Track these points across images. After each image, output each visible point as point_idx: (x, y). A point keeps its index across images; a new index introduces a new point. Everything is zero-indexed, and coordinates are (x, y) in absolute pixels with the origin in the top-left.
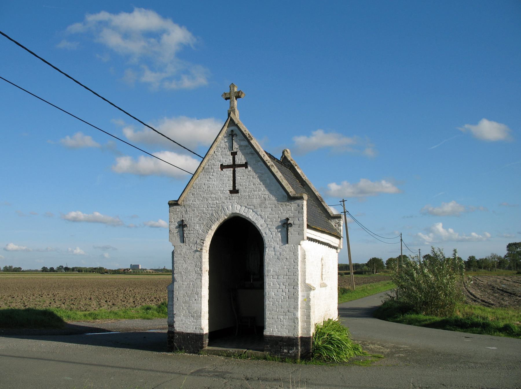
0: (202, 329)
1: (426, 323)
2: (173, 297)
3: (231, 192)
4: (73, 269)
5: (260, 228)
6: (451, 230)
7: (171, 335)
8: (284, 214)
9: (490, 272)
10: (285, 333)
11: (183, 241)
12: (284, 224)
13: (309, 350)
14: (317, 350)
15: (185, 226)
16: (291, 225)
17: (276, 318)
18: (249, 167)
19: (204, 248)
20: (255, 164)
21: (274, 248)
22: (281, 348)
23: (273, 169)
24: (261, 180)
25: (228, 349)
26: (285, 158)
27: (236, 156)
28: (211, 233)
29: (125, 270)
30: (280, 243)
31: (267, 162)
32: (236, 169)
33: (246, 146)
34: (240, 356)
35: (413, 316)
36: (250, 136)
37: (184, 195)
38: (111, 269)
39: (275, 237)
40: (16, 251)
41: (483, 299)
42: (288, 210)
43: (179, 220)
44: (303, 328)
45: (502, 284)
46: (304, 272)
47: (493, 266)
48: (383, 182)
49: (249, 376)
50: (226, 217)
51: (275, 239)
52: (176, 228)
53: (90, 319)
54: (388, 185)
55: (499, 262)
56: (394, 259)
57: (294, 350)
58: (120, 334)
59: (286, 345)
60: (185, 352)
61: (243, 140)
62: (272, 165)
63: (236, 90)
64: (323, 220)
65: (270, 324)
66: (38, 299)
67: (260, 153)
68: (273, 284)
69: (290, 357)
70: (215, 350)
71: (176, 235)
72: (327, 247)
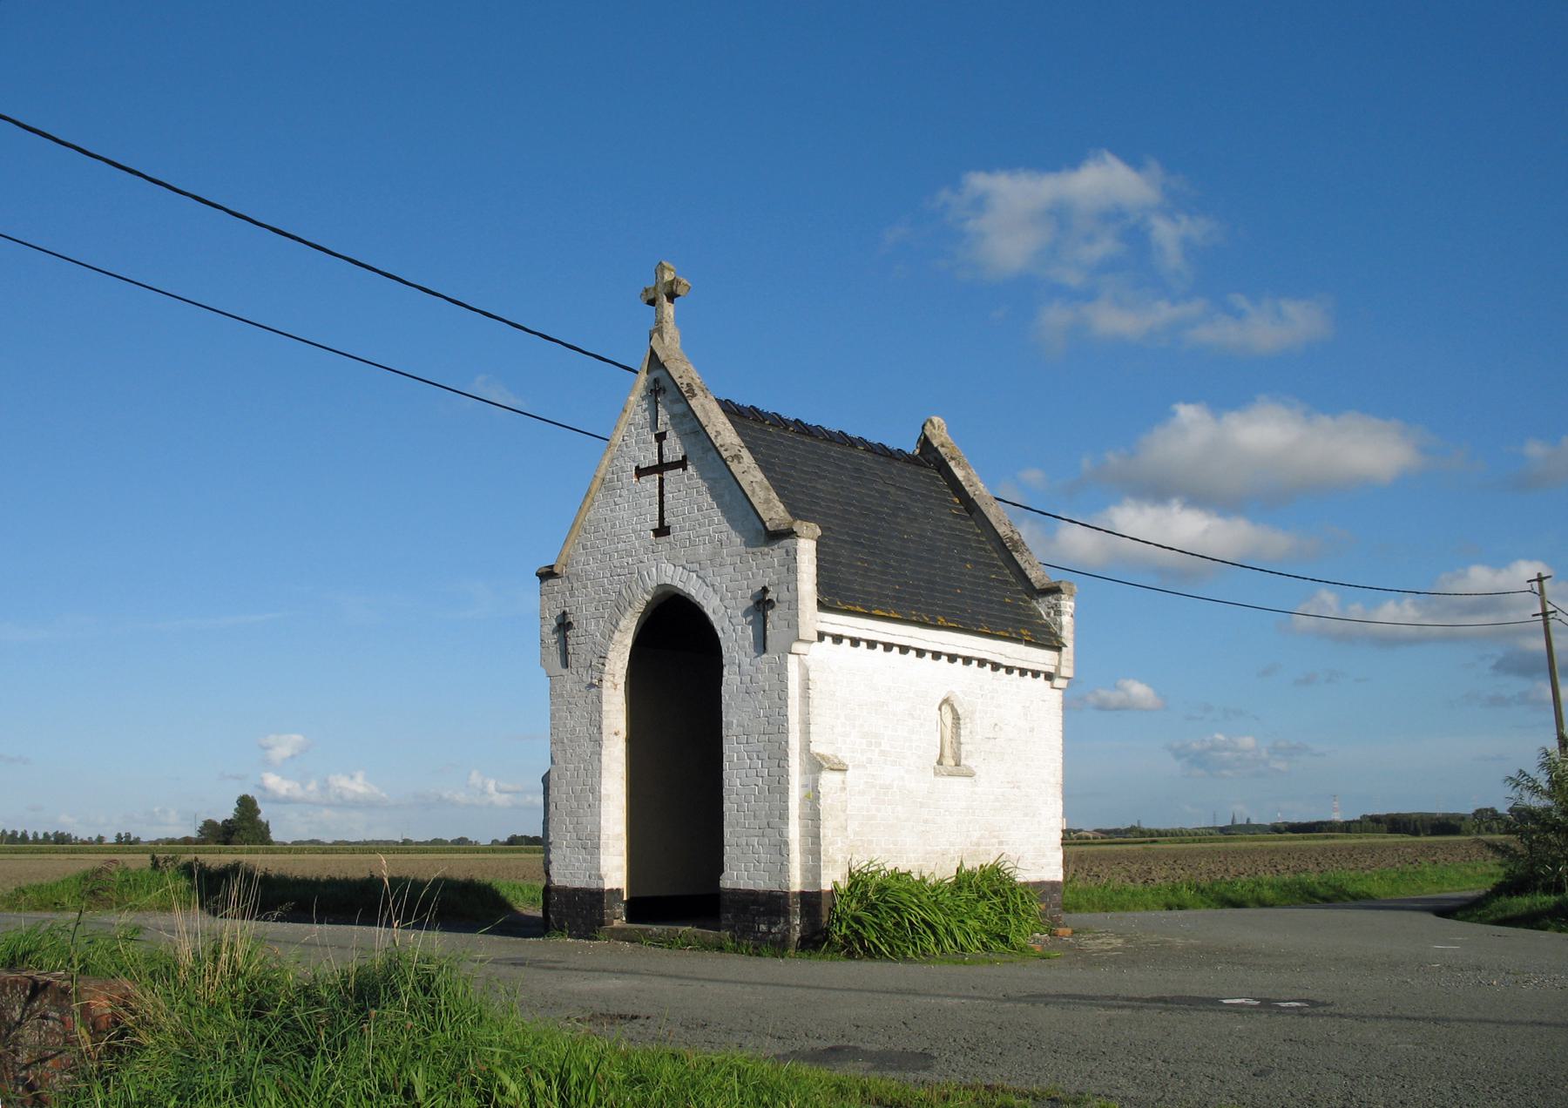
0: (600, 878)
11: (566, 664)
19: (606, 677)
23: (734, 466)
24: (714, 498)
26: (925, 443)
30: (750, 651)
42: (762, 568)
50: (649, 598)
60: (570, 936)
63: (668, 277)
69: (773, 943)
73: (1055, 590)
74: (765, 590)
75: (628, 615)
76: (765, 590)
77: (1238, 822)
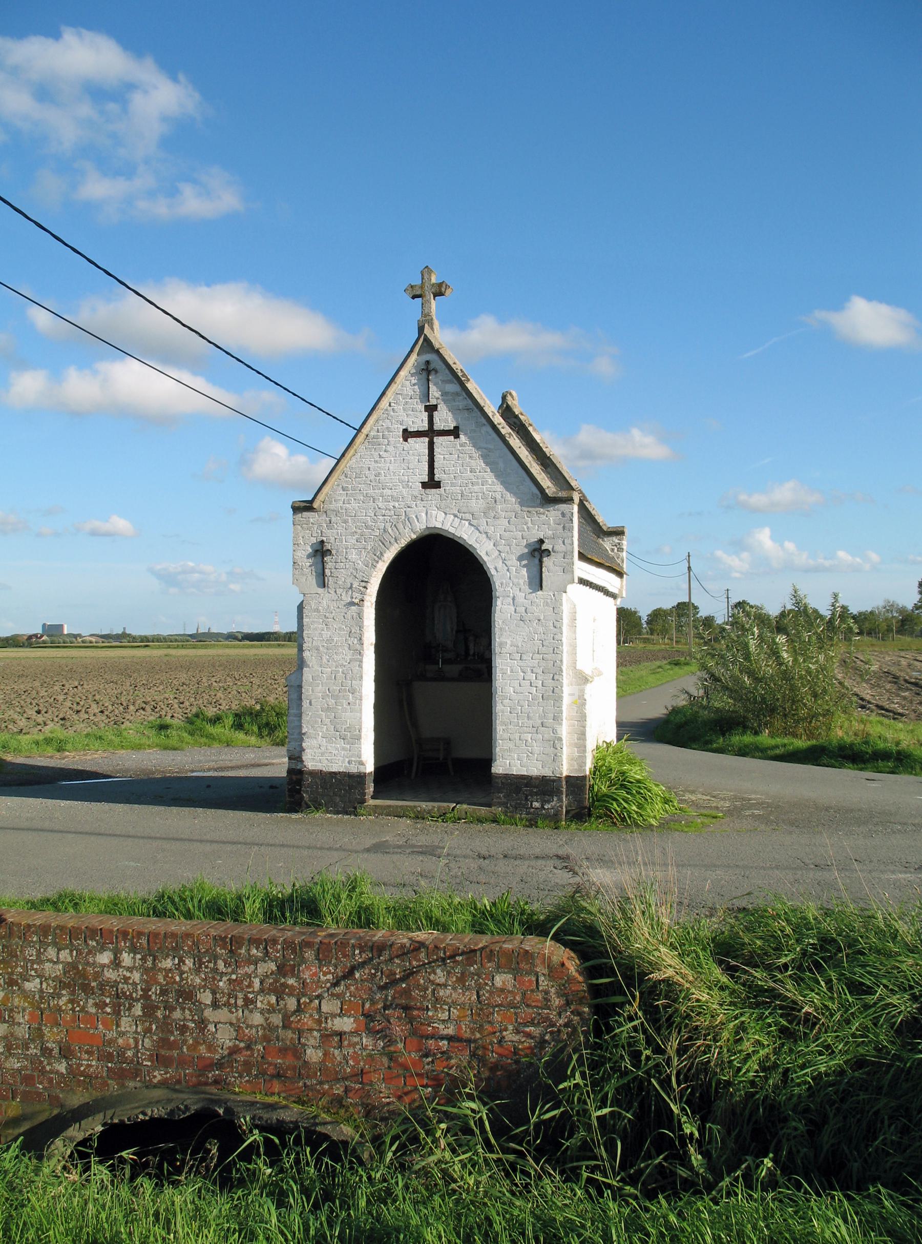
0: (362, 763)
1: (777, 752)
2: (301, 699)
3: (425, 485)
5: (485, 558)
6: (790, 546)
7: (294, 777)
8: (534, 532)
9: (881, 642)
10: (534, 769)
12: (535, 550)
15: (329, 552)
16: (548, 552)
17: (517, 738)
19: (367, 598)
20: (475, 431)
21: (514, 599)
22: (527, 799)
24: (487, 464)
25: (417, 804)
27: (435, 413)
28: (382, 567)
29: (30, 637)
31: (499, 427)
32: (435, 439)
33: (457, 394)
34: (443, 816)
35: (748, 739)
39: (516, 577)
41: (880, 703)
42: (542, 524)
43: (314, 540)
45: (914, 670)
46: (574, 647)
47: (889, 630)
48: (636, 433)
49: (484, 852)
50: (414, 536)
51: (516, 581)
52: (309, 557)
53: (50, 751)
54: (649, 440)
55: (902, 621)
56: (665, 611)
57: (554, 802)
58: (165, 780)
59: (536, 794)
61: (450, 382)
63: (434, 280)
64: (599, 540)
65: (504, 750)
67: (486, 409)
68: (512, 671)
69: (546, 817)
70: (389, 806)
71: (307, 571)
72: (600, 595)
74: (541, 541)
76: (541, 541)
77: (201, 631)
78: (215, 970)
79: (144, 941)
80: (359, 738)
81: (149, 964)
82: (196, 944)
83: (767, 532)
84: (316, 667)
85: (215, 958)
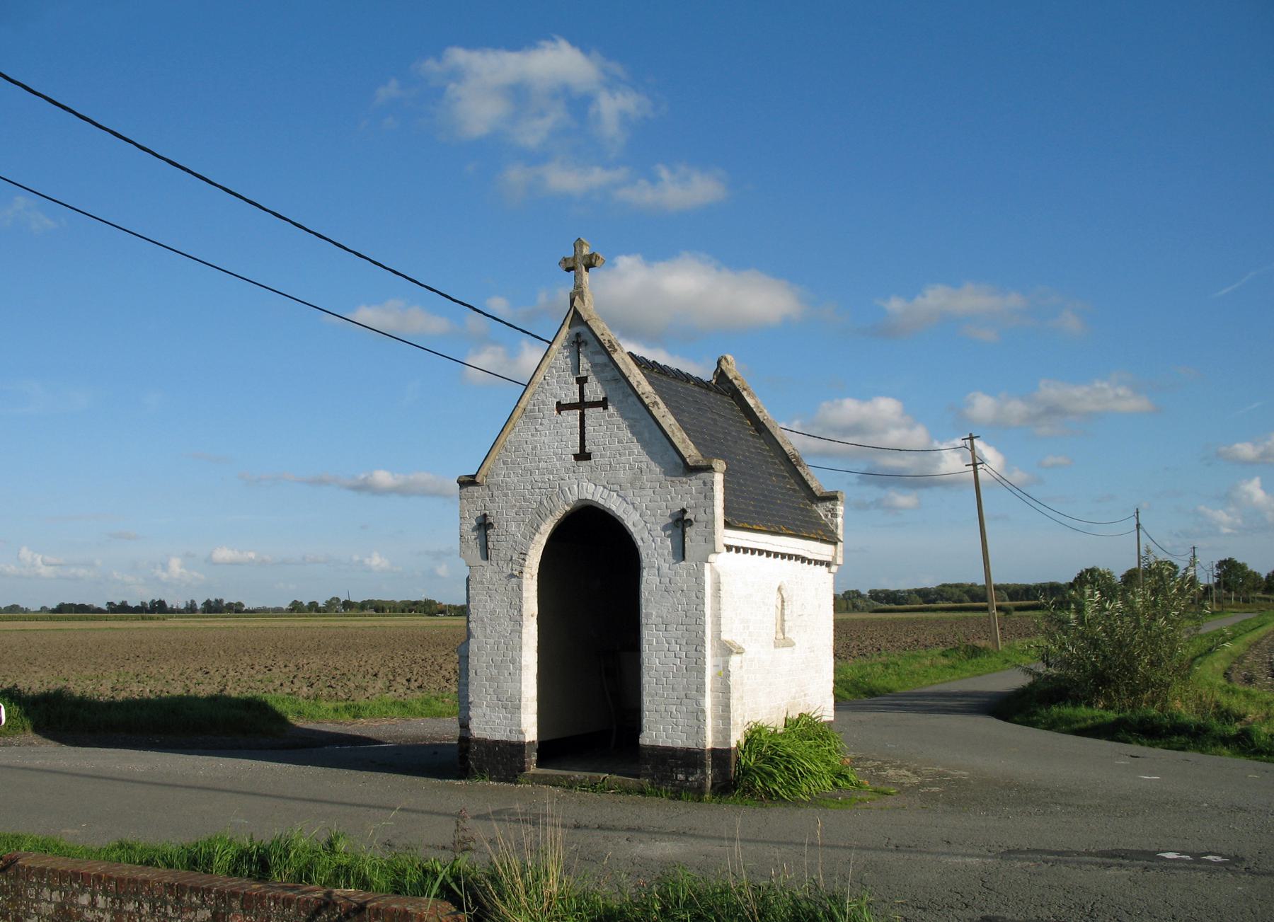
0: (521, 732)
1: (1082, 725)
3: (578, 457)
4: (363, 606)
11: (486, 556)
12: (677, 521)
13: (745, 775)
14: (744, 774)
18: (610, 408)
19: (526, 570)
23: (655, 411)
24: (633, 434)
26: (721, 375)
28: (541, 541)
33: (605, 365)
34: (593, 787)
35: (1067, 711)
36: (612, 345)
37: (487, 465)
38: (453, 603)
40: (233, 564)
42: (684, 493)
44: (716, 732)
50: (568, 508)
60: (491, 779)
62: (655, 403)
63: (586, 251)
66: (260, 677)
67: (631, 379)
69: (691, 789)
73: (832, 498)
74: (684, 511)
75: (548, 521)
76: (684, 511)
78: (165, 915)
79: (113, 885)
80: (518, 708)
81: (117, 906)
82: (151, 890)
83: (1256, 482)
84: (481, 638)
85: (165, 903)
